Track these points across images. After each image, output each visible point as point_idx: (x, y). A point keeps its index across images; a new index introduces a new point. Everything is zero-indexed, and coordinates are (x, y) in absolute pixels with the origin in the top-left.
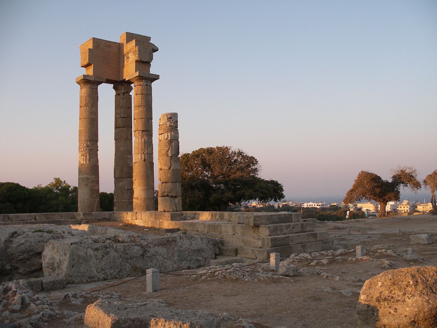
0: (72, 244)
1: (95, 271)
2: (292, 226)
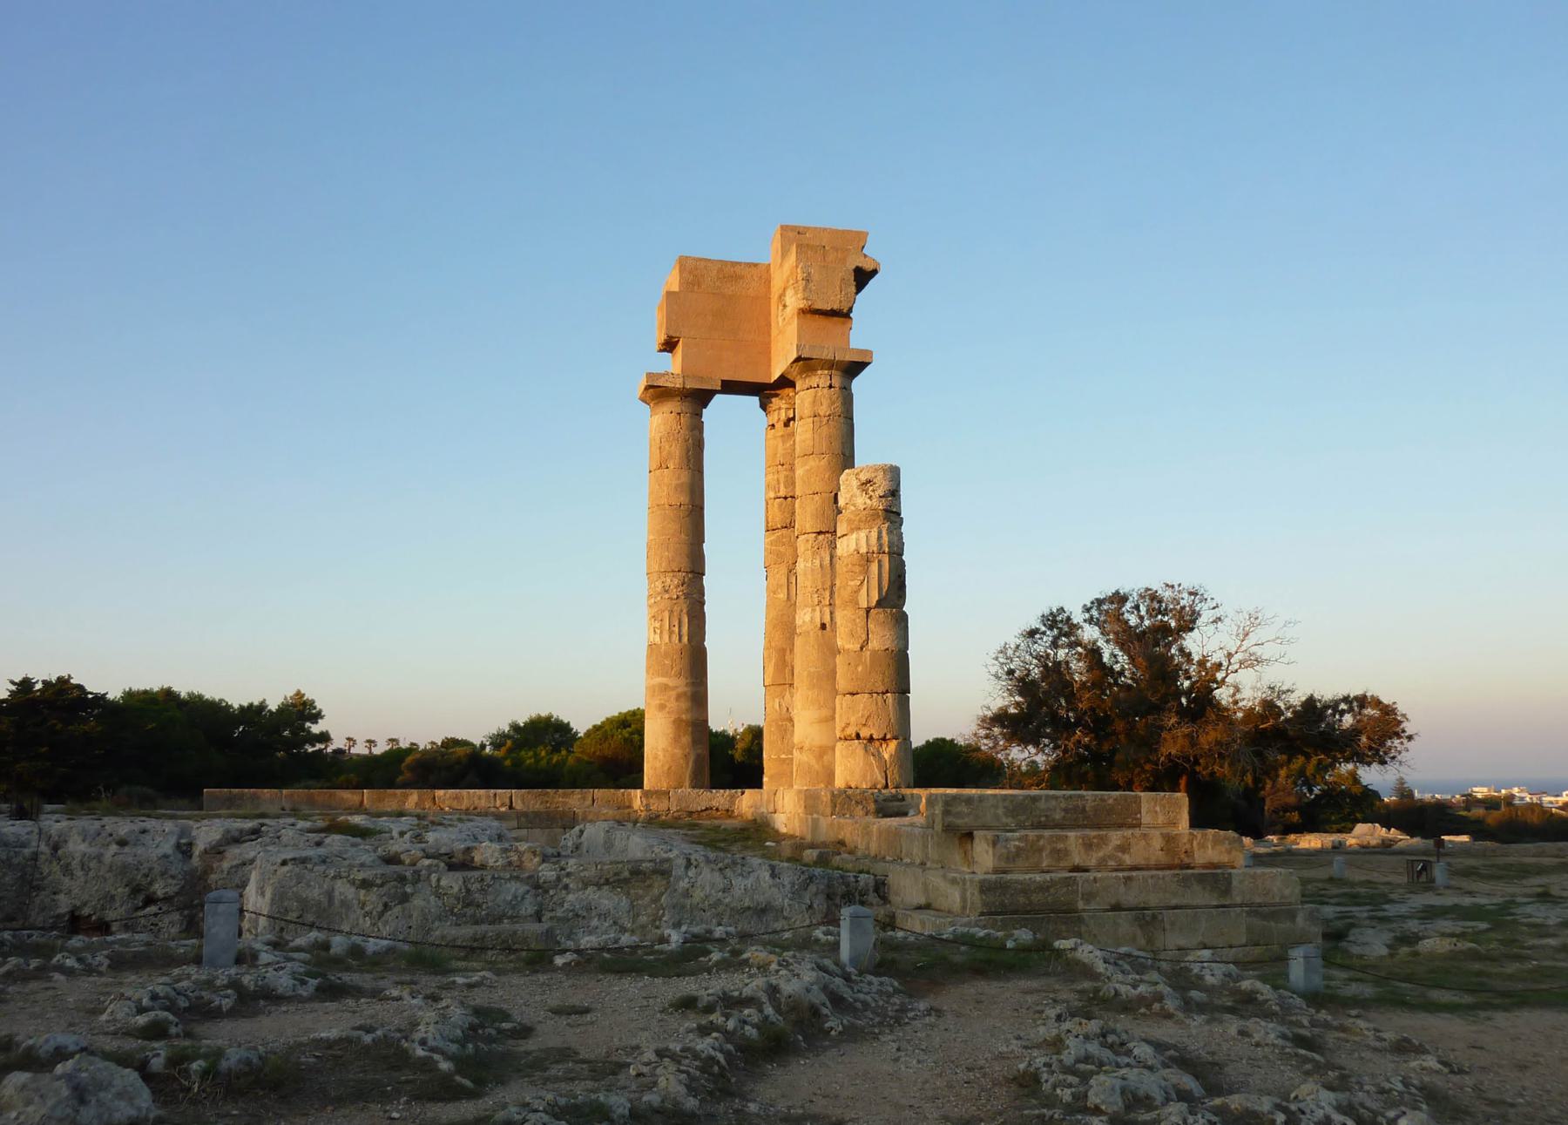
0: (284, 863)
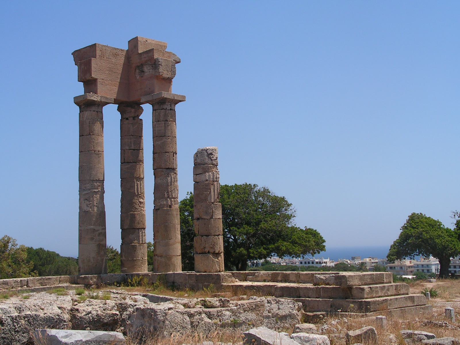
2: (386, 288)
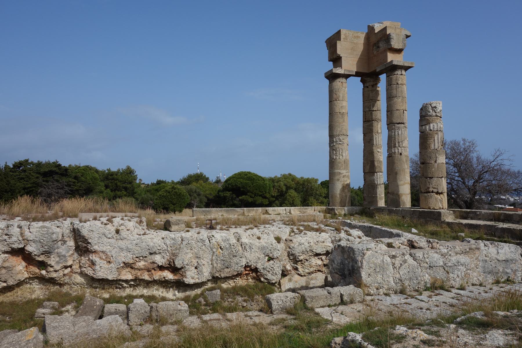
1: (392, 282)
